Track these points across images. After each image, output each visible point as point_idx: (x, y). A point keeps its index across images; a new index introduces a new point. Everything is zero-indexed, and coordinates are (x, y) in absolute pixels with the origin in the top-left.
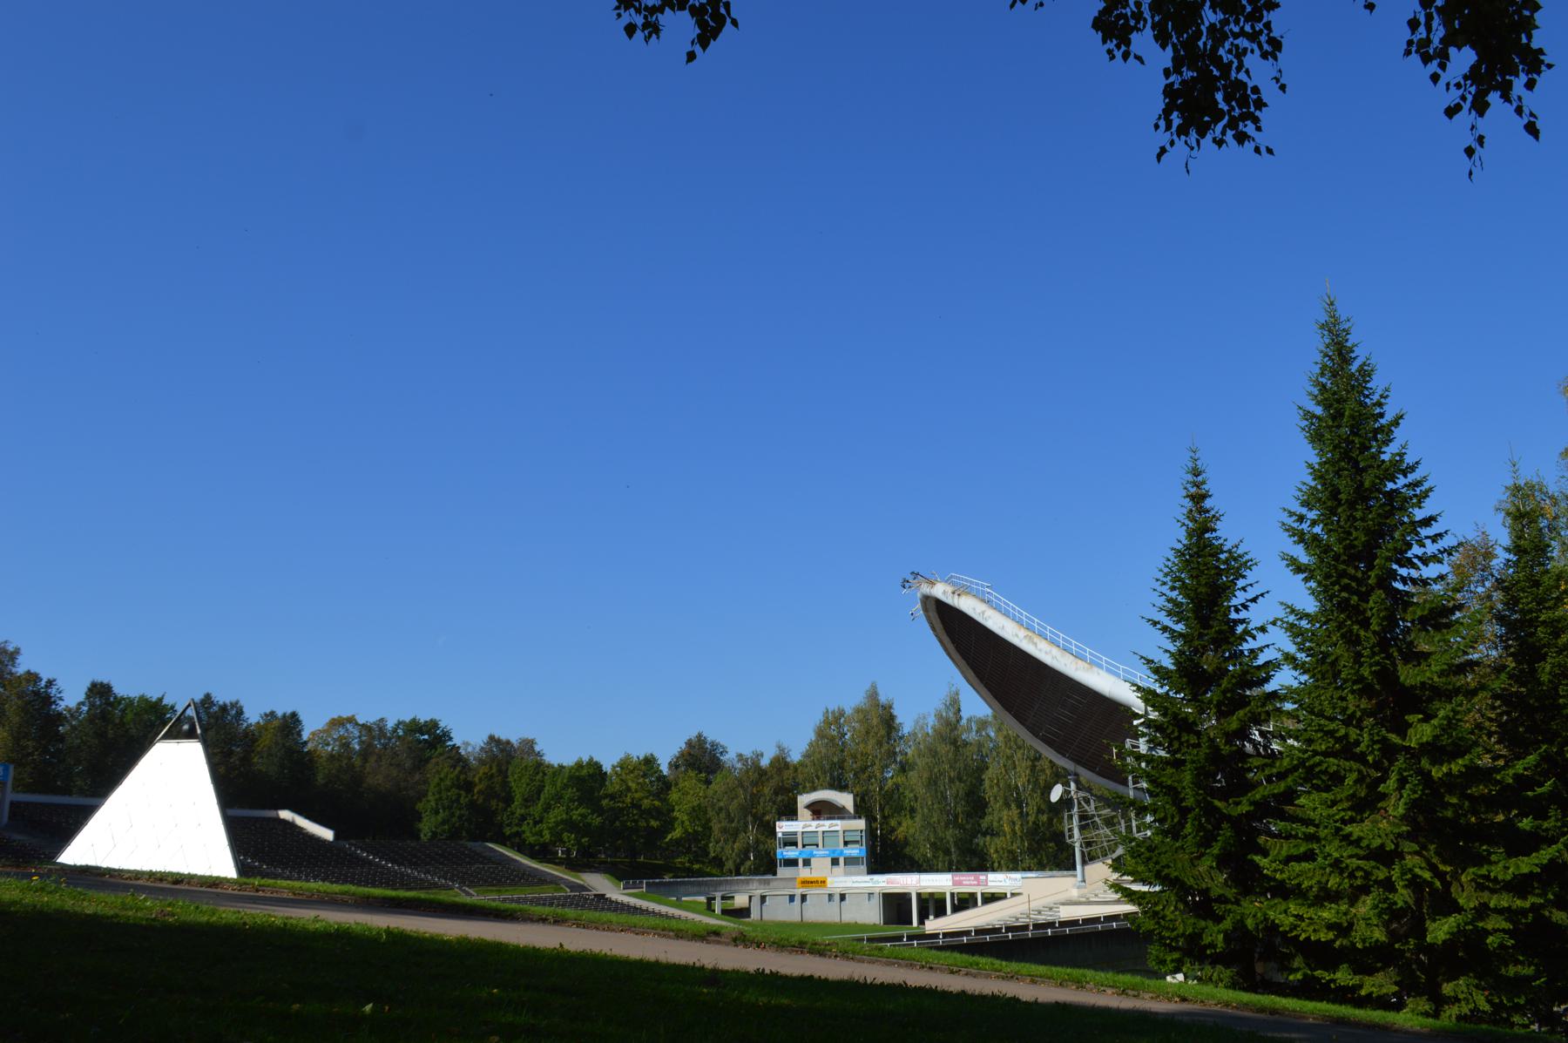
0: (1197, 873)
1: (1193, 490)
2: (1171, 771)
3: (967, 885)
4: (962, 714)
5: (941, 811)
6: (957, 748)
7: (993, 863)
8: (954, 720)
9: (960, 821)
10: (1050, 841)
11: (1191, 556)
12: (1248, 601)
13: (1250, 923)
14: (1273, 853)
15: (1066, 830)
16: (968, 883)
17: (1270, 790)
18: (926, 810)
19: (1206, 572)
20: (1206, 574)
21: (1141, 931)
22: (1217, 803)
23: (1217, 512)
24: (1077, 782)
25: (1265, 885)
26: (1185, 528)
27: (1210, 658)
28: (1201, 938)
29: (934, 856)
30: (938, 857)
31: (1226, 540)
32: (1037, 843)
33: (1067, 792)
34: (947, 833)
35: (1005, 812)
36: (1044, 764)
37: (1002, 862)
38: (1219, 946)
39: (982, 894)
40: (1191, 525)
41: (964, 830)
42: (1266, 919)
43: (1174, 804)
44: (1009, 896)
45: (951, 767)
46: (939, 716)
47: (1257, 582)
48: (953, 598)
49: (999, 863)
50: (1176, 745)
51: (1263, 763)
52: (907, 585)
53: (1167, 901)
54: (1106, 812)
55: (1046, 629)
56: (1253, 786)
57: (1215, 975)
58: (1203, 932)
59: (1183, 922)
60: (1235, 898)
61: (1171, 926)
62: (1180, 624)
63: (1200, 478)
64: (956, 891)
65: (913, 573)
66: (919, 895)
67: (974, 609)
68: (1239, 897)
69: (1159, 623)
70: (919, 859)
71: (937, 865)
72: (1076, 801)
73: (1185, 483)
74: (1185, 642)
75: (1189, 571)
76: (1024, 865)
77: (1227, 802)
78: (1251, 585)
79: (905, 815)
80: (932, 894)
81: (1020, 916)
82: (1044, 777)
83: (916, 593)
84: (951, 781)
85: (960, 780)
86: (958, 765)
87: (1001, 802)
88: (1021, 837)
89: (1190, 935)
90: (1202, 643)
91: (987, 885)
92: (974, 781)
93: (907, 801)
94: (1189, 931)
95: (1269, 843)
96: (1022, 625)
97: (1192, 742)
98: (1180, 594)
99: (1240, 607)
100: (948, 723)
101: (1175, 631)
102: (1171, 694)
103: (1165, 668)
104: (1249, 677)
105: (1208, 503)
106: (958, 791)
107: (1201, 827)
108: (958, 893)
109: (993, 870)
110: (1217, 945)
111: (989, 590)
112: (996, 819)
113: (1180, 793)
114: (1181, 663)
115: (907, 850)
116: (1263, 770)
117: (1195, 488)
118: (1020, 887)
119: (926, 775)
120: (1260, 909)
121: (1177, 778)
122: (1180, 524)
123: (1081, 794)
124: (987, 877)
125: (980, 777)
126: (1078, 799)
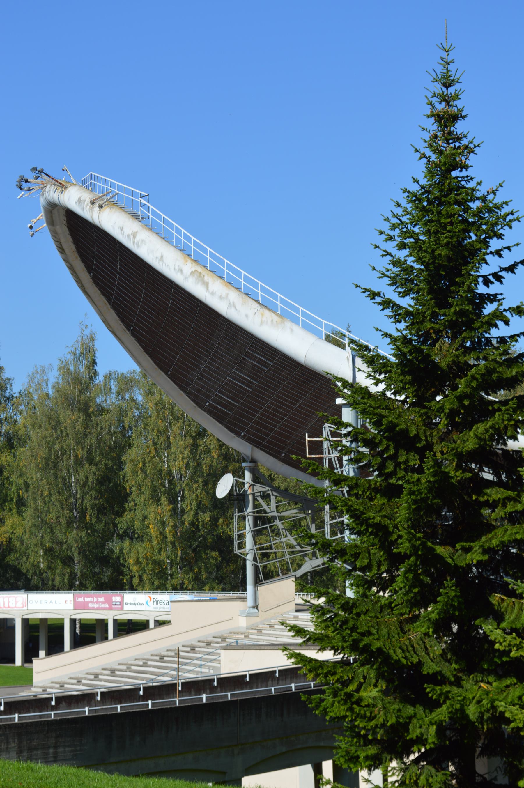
0: (407, 642)
1: (441, 107)
2: (381, 502)
3: (93, 609)
4: (98, 368)
5: (62, 504)
6: (88, 416)
7: (132, 577)
8: (86, 376)
9: (88, 518)
10: (213, 549)
11: (430, 202)
12: (503, 269)
13: (472, 711)
14: (509, 618)
15: (235, 537)
16: (96, 606)
17: (511, 534)
18: (40, 503)
19: (448, 228)
20: (449, 231)
21: (327, 718)
22: (440, 550)
23: (471, 142)
24: (254, 471)
25: (496, 660)
26: (425, 160)
27: (445, 348)
28: (407, 731)
29: (49, 568)
30: (55, 568)
31: (479, 184)
32: (194, 551)
33: (237, 485)
34: (69, 535)
35: (152, 508)
36: (209, 442)
37: (145, 577)
38: (430, 741)
39: (115, 621)
40: (433, 157)
41: (94, 531)
42: (494, 708)
43: (382, 547)
44: (152, 625)
45: (78, 443)
46: (65, 370)
47: (517, 245)
48: (92, 210)
49: (140, 577)
50: (390, 467)
51: (506, 495)
52: (25, 186)
53: (365, 678)
54: (292, 512)
55: (222, 262)
56: (490, 528)
57: (422, 778)
58: (410, 722)
59: (384, 708)
60: (455, 676)
61: (368, 714)
62: (407, 298)
63: (451, 90)
64: (78, 617)
65: (34, 169)
66: (25, 622)
67: (122, 229)
68: (460, 675)
69: (378, 294)
70: (28, 571)
71: (53, 580)
72: (251, 497)
73: (430, 95)
74: (412, 324)
75: (425, 224)
76: (175, 582)
77: (454, 547)
78: (509, 248)
79: (10, 510)
80: (44, 621)
81: (166, 653)
82: (208, 461)
83: (39, 197)
84: (79, 462)
85: (91, 461)
86: (88, 441)
87: (147, 493)
88: (173, 543)
89: (392, 726)
90: (437, 326)
91: (122, 609)
92: (110, 463)
93: (14, 489)
94: (392, 720)
95: (505, 604)
96: (189, 255)
97: (412, 463)
98: (411, 255)
99: (491, 278)
100: (77, 381)
101: (399, 307)
102: (389, 394)
103: (384, 358)
104: (495, 376)
105: (459, 127)
106: (87, 477)
107: (416, 581)
108: (80, 619)
109: (132, 588)
110: (426, 740)
111: (145, 202)
112: (139, 516)
113: (391, 534)
114: (404, 354)
115: (11, 559)
116: (504, 506)
117: (444, 104)
118: (168, 613)
119: (42, 453)
120: (487, 693)
121: (389, 511)
122: (418, 155)
123: (259, 488)
124: (122, 598)
125: (119, 457)
126: (253, 494)
